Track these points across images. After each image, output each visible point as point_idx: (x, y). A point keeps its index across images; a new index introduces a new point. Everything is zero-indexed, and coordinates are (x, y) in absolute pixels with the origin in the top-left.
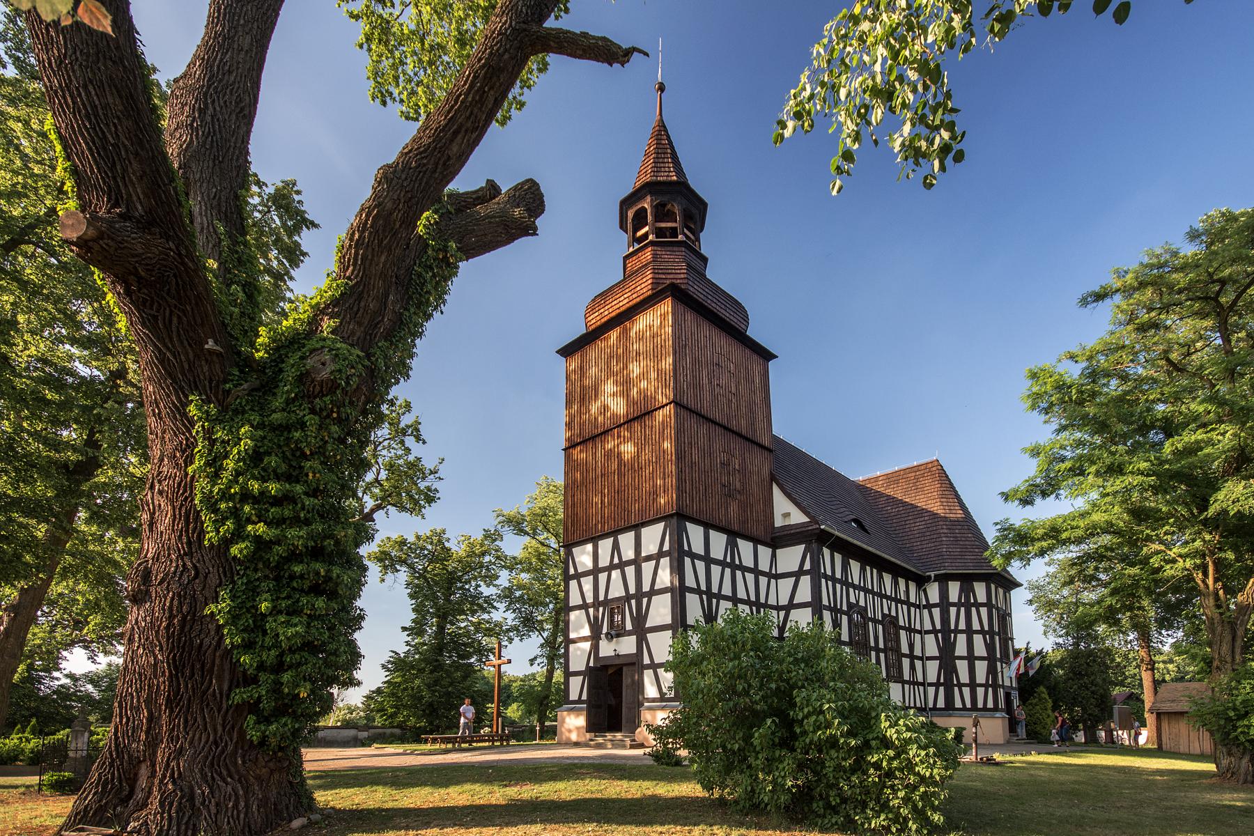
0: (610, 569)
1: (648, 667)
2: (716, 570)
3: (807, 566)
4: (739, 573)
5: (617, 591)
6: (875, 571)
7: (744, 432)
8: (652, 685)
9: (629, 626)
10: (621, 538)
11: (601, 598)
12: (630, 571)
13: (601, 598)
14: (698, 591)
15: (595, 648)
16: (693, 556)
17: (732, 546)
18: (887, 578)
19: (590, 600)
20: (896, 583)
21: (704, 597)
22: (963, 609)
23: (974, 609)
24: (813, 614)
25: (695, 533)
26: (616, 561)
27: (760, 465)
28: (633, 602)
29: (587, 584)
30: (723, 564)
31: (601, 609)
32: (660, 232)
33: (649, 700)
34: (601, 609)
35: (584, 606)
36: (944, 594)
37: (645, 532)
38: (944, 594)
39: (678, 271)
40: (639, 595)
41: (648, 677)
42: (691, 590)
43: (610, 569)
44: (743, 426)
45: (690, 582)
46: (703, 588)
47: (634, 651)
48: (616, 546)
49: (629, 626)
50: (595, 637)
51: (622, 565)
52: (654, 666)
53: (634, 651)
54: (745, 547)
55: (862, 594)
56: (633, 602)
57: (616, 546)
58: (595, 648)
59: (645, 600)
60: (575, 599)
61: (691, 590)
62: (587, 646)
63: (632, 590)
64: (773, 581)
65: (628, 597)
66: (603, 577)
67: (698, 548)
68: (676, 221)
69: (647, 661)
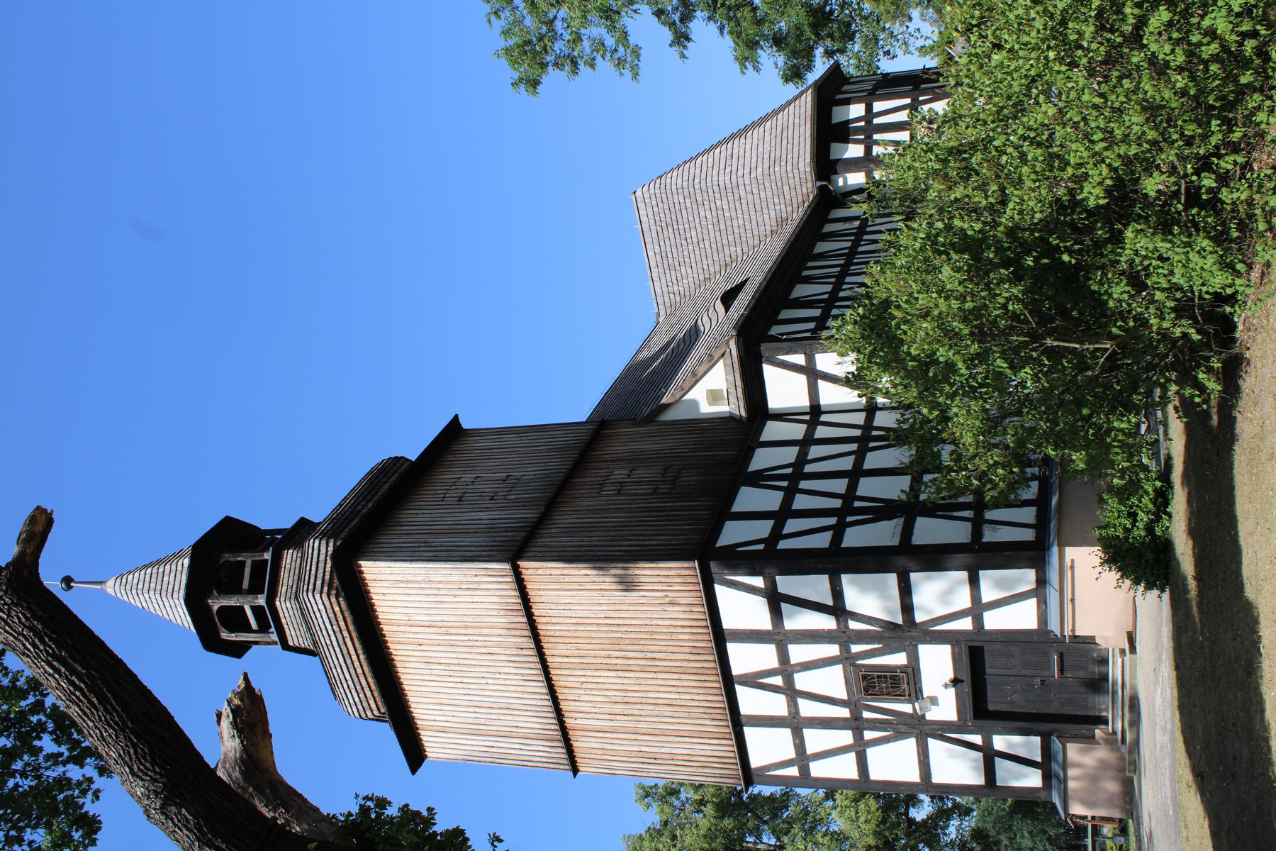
0: (791, 693)
1: (978, 620)
2: (801, 502)
3: (799, 359)
4: (809, 468)
5: (833, 681)
6: (810, 264)
7: (531, 514)
8: (996, 530)
9: (899, 659)
10: (737, 669)
11: (844, 713)
12: (798, 653)
13: (844, 713)
14: (839, 531)
15: (941, 730)
16: (777, 534)
17: (760, 479)
18: (801, 291)
19: (846, 737)
20: (822, 256)
21: (849, 519)
22: (876, 137)
23: (876, 121)
24: (887, 429)
25: (733, 533)
26: (777, 681)
27: (624, 443)
28: (855, 648)
29: (815, 740)
30: (790, 493)
31: (867, 715)
32: (255, 589)
33: (1043, 618)
34: (867, 715)
35: (860, 750)
36: (854, 164)
37: (729, 621)
38: (854, 164)
39: (320, 551)
40: (842, 637)
41: (994, 621)
42: (837, 538)
43: (791, 693)
44: (557, 466)
45: (822, 541)
46: (832, 521)
47: (947, 649)
48: (753, 681)
49: (899, 659)
50: (921, 729)
51: (786, 668)
52: (977, 609)
53: (947, 649)
54: (762, 459)
55: (848, 279)
56: (855, 648)
57: (753, 681)
58: (941, 730)
59: (853, 625)
60: (844, 768)
61: (837, 538)
62: (936, 747)
63: (833, 650)
64: (824, 418)
65: (846, 659)
66: (808, 709)
67: (763, 529)
68: (245, 561)
69: (966, 624)
